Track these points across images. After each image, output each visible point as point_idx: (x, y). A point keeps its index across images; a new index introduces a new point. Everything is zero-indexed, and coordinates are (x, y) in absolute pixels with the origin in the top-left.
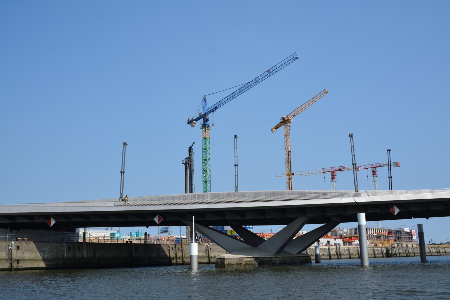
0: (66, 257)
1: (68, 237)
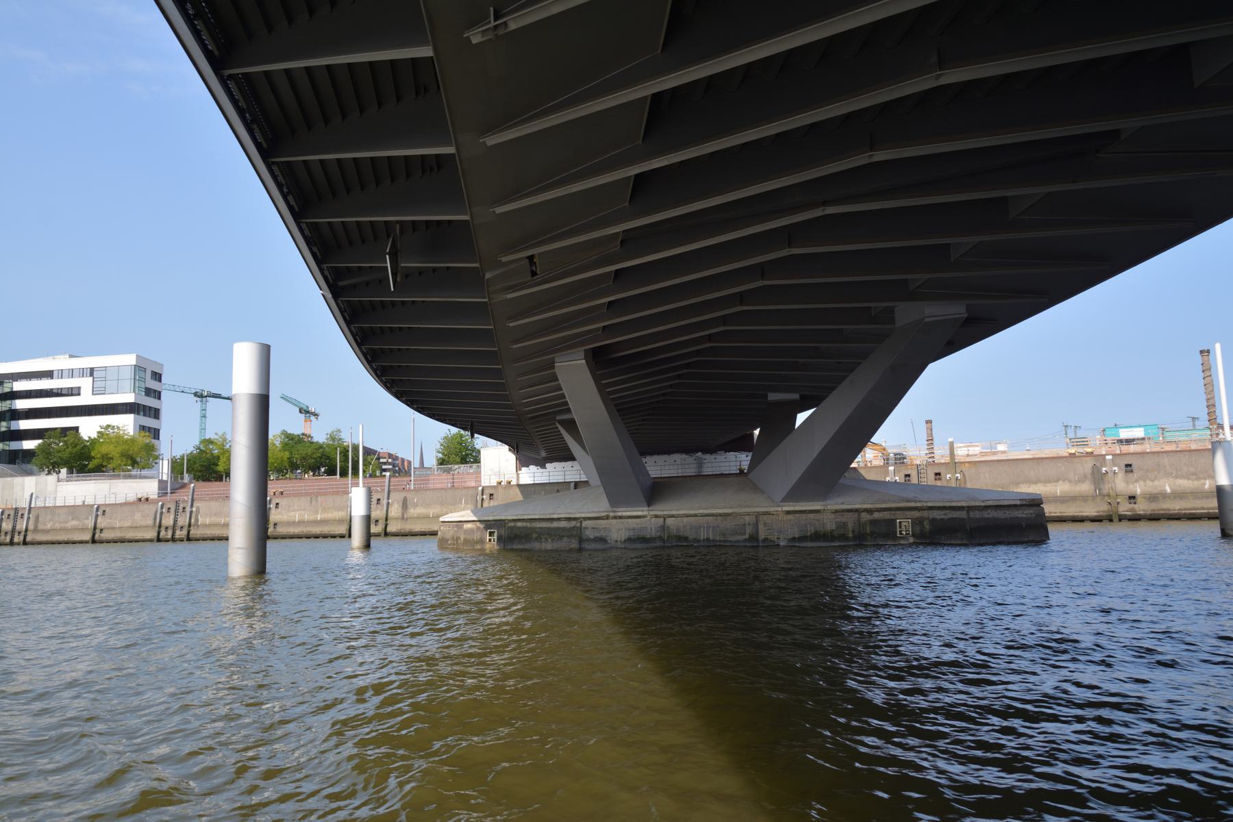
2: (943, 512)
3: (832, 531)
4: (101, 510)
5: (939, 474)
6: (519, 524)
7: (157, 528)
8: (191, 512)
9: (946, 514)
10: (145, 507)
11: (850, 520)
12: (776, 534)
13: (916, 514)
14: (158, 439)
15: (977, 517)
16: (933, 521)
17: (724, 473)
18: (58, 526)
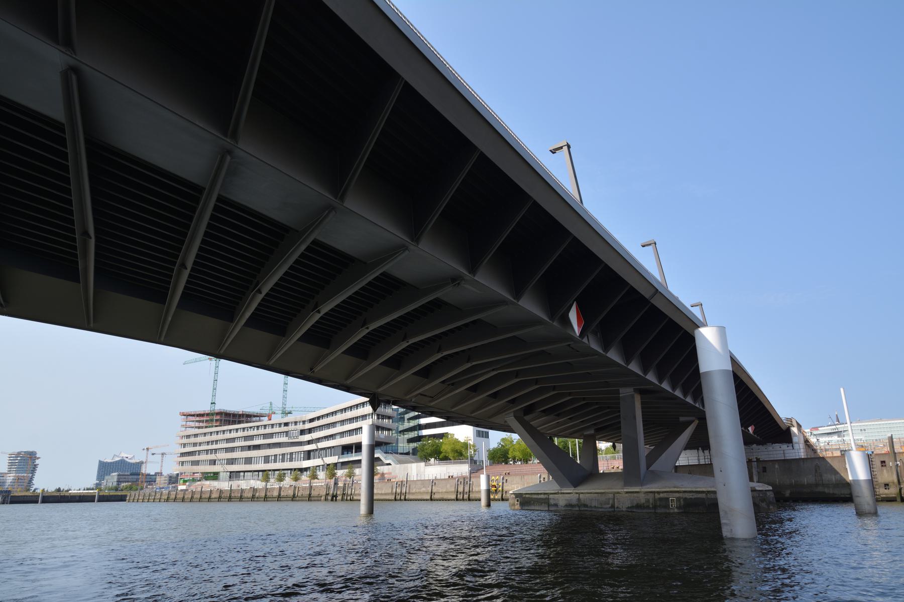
0: (835, 480)
1: (782, 452)
2: (691, 494)
3: (644, 504)
4: (433, 482)
5: (884, 462)
6: (527, 496)
7: (456, 493)
8: (470, 484)
9: (692, 496)
10: (451, 481)
11: (651, 496)
12: (621, 504)
13: (677, 495)
14: (488, 438)
15: (712, 497)
16: (685, 499)
17: (766, 459)
18: (417, 491)
